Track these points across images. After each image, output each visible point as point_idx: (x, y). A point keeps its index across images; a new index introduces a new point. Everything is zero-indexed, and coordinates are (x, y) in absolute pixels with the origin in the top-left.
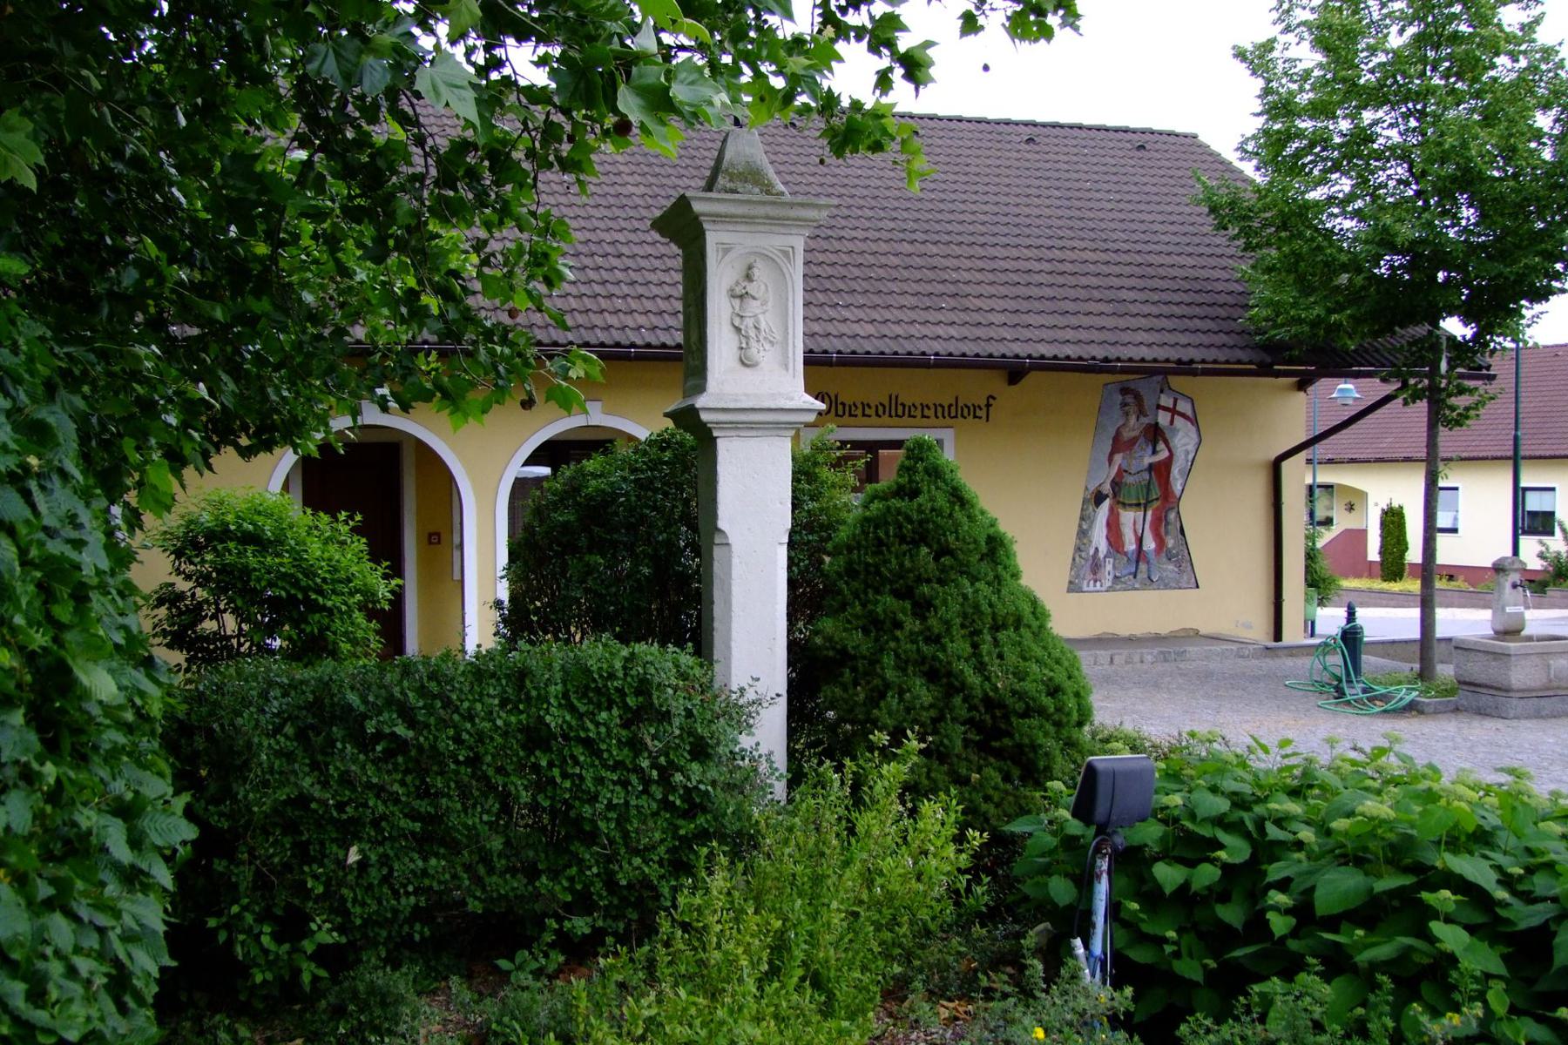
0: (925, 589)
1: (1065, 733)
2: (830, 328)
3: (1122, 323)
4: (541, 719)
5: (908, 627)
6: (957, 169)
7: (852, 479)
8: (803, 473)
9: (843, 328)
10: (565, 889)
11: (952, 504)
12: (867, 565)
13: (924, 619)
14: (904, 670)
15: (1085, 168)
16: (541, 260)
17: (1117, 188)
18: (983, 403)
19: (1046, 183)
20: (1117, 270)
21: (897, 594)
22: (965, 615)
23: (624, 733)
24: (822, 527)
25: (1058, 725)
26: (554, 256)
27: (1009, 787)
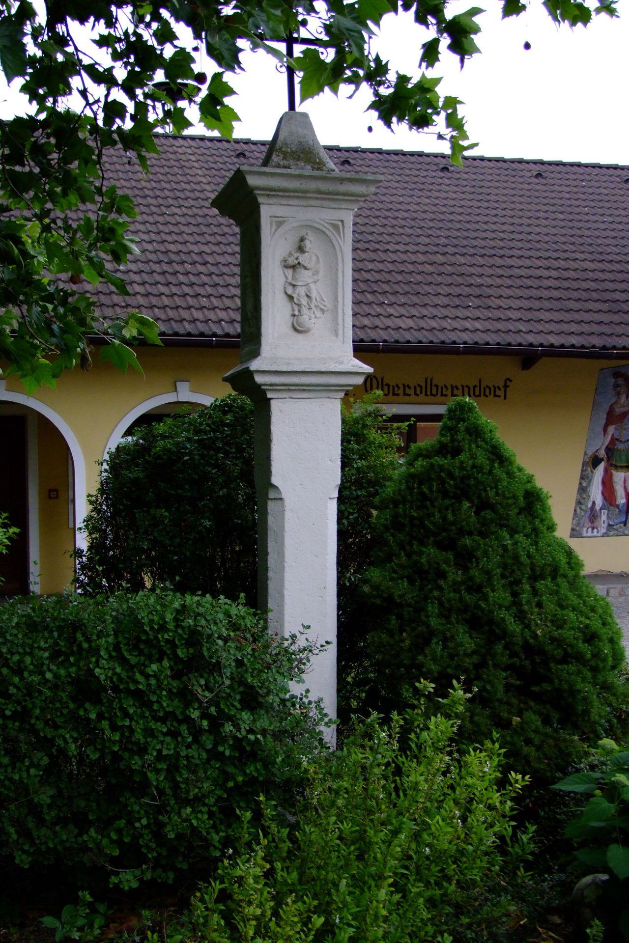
0: (468, 541)
1: (600, 678)
2: (377, 322)
3: (616, 318)
4: (90, 672)
5: (451, 576)
6: (480, 197)
7: (398, 441)
8: (353, 436)
9: (388, 322)
10: (112, 841)
11: (492, 461)
12: (413, 518)
13: (466, 569)
14: (448, 618)
15: (582, 196)
16: (108, 235)
17: (609, 212)
18: (501, 384)
19: (552, 209)
20: (611, 276)
21: (440, 546)
22: (504, 566)
23: (175, 683)
24: (370, 483)
25: (595, 670)
26: (120, 231)
27: (549, 730)
